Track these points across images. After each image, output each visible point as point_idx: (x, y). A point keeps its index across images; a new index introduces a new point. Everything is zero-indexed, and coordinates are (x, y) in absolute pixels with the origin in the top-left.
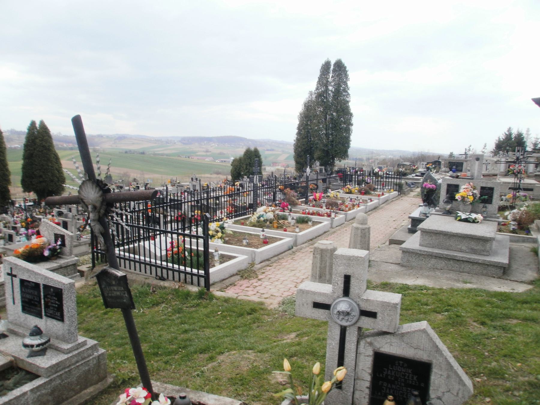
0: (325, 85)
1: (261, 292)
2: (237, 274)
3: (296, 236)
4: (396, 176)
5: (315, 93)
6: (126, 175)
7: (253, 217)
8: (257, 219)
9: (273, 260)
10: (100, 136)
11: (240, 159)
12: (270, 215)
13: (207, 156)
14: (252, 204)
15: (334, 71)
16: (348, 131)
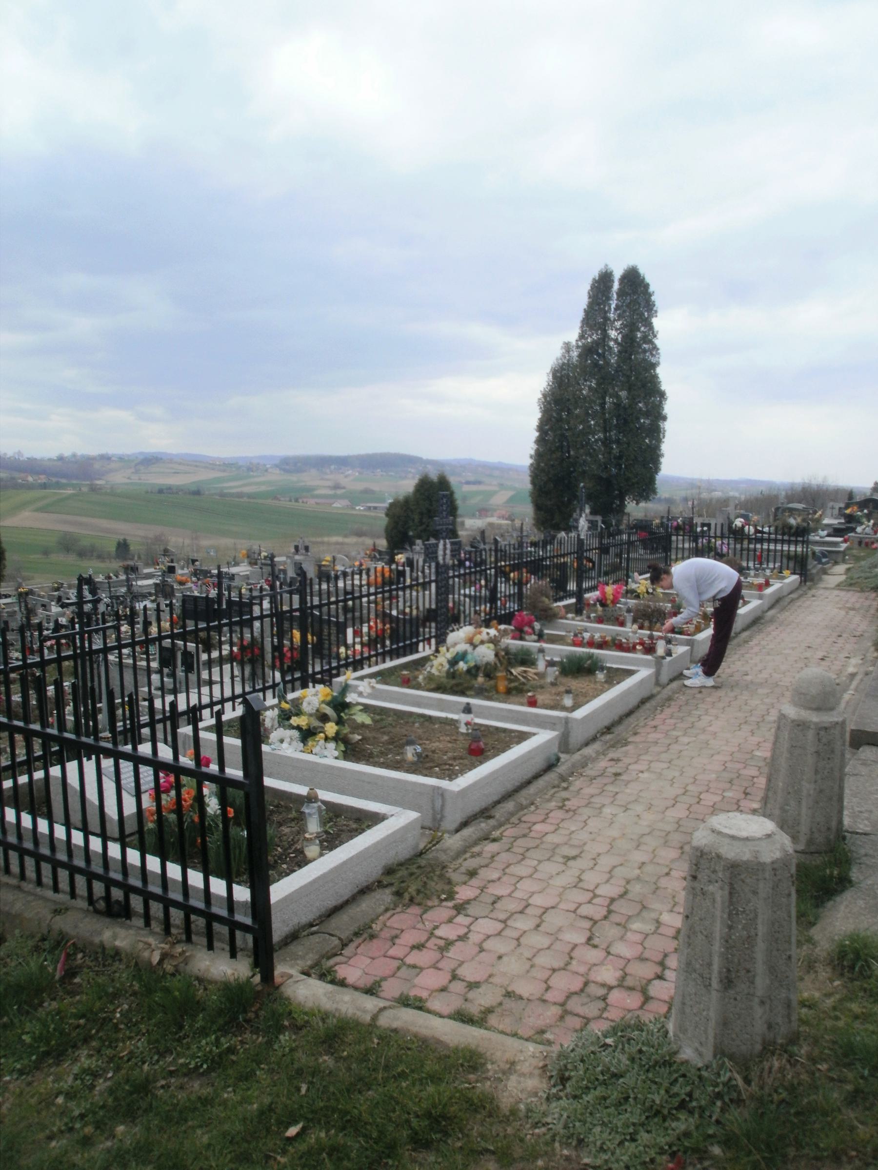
0: (600, 328)
1: (469, 972)
2: (380, 884)
3: (567, 721)
4: (779, 537)
5: (578, 347)
6: (158, 539)
7: (436, 662)
8: (447, 666)
9: (500, 813)
10: (106, 458)
11: (407, 501)
12: (486, 654)
13: (336, 497)
14: (435, 611)
15: (621, 293)
16: (655, 432)
